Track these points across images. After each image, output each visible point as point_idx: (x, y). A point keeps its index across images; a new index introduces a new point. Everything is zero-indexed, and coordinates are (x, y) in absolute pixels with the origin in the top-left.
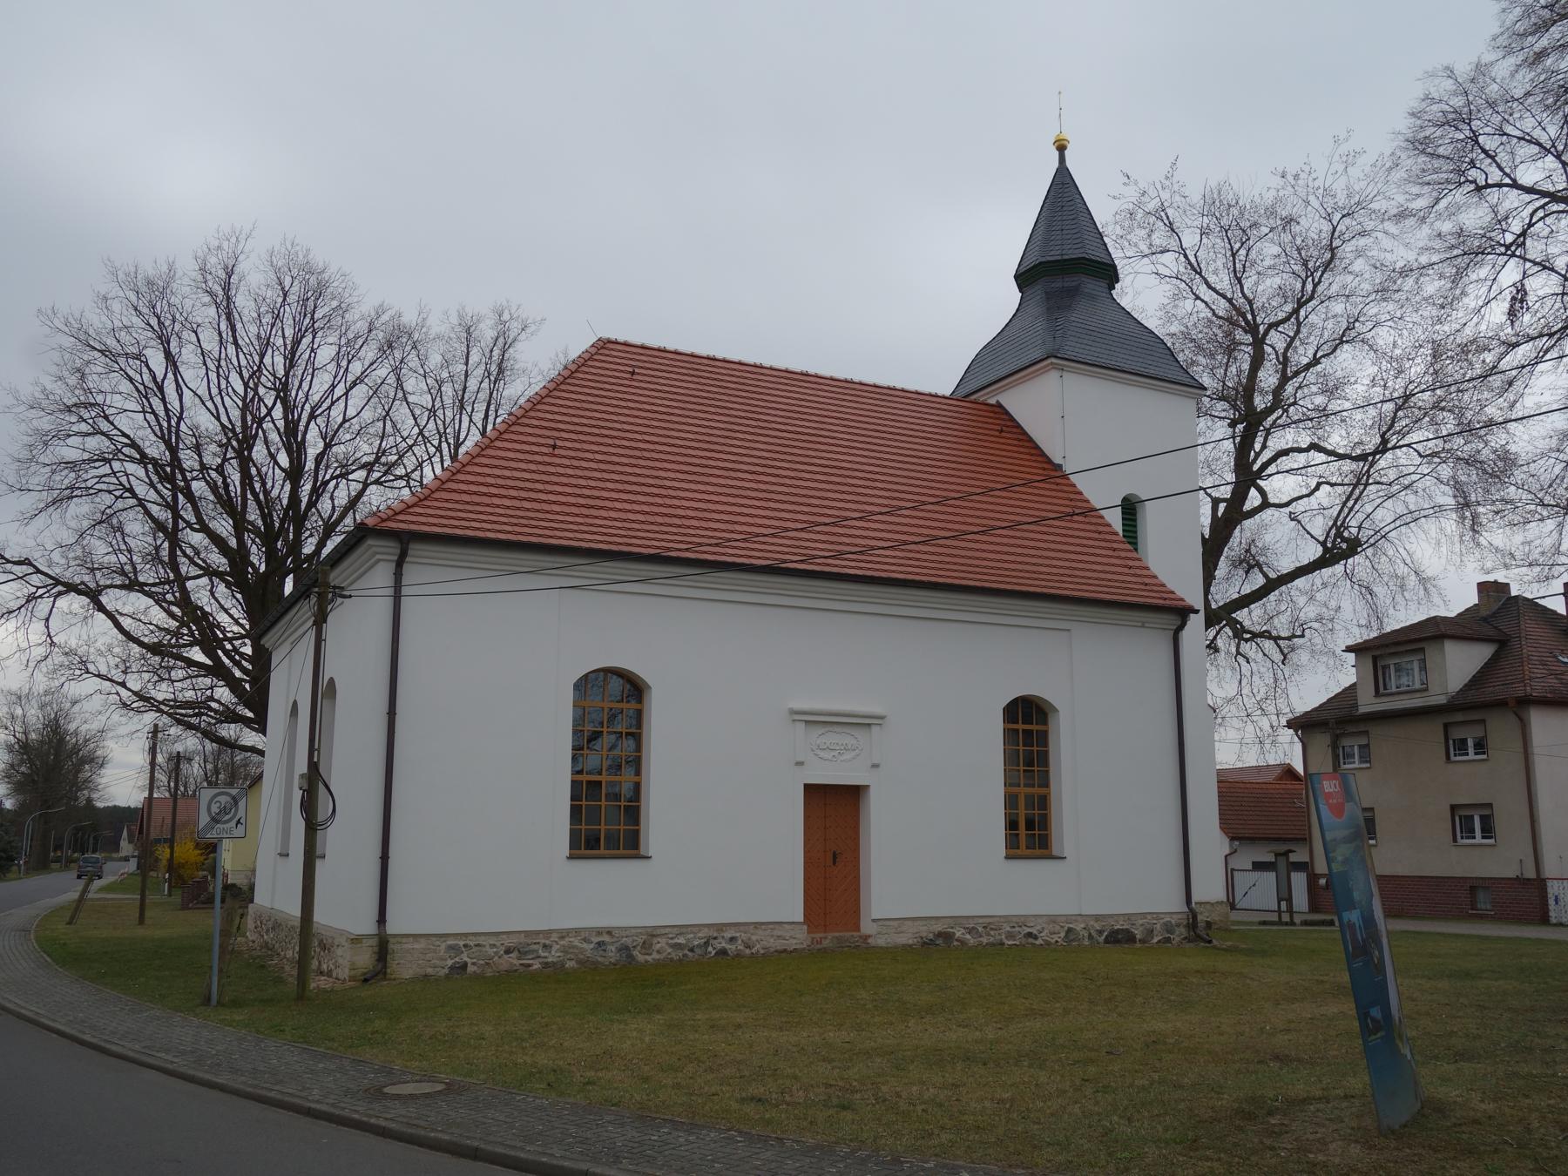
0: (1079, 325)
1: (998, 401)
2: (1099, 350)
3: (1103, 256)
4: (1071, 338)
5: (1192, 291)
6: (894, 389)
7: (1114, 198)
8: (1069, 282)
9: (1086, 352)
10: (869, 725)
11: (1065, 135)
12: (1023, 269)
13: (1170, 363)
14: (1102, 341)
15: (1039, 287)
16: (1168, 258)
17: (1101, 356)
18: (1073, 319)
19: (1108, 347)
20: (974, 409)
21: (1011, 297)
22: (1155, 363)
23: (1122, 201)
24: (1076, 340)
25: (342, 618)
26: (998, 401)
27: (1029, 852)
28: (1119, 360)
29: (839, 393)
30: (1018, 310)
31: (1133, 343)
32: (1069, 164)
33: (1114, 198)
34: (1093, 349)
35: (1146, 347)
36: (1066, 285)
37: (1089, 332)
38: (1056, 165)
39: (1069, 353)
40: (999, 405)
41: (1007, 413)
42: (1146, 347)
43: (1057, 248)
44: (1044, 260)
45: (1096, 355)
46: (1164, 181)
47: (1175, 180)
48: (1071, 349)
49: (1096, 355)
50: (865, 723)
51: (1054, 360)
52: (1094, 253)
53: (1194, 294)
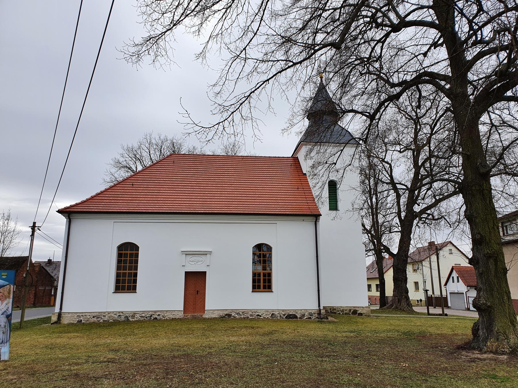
10: (207, 254)
27: (264, 290)
50: (205, 254)
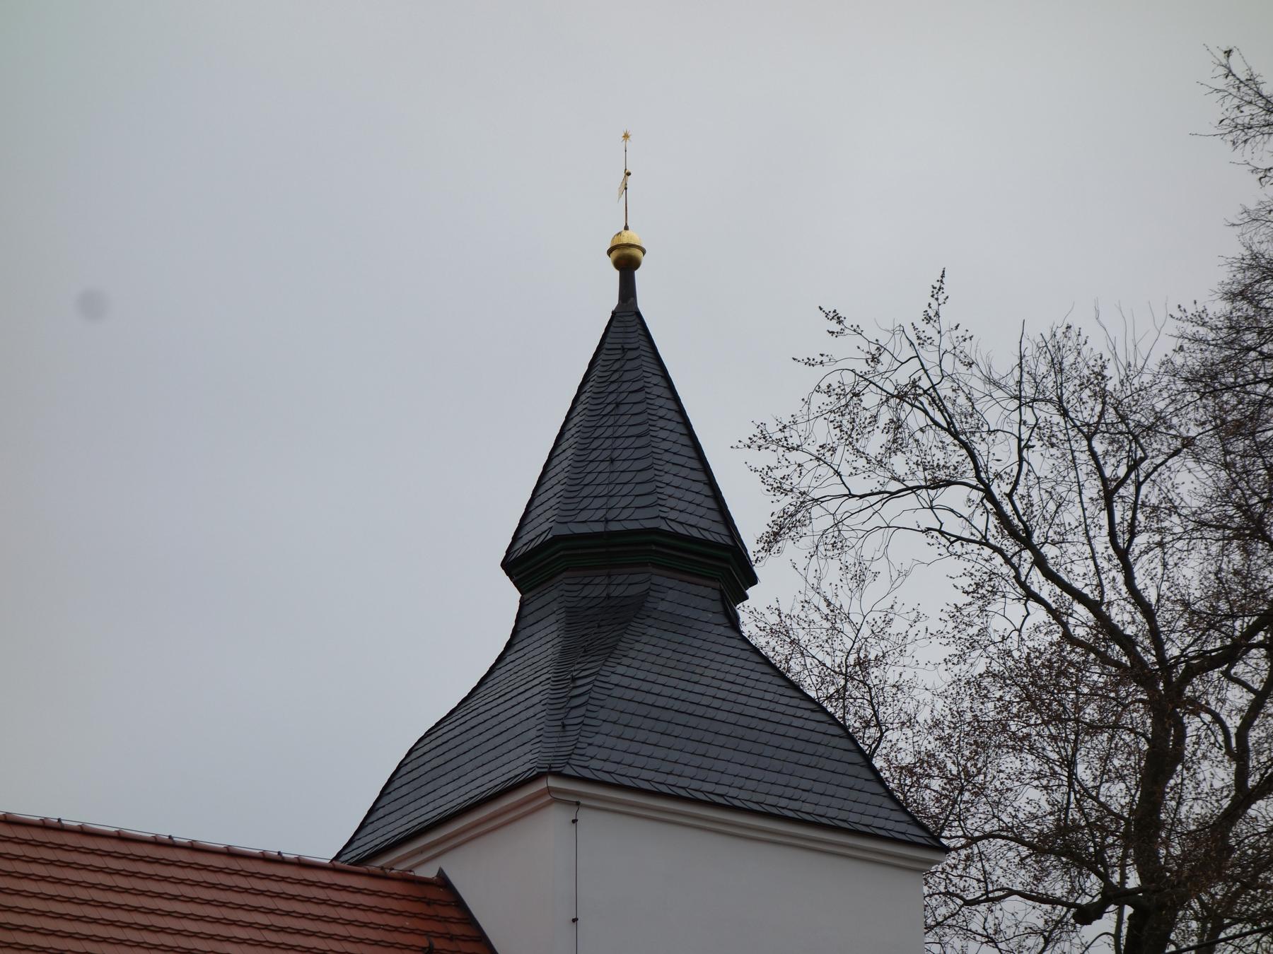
0: (629, 694)
1: (441, 874)
2: (674, 755)
3: (703, 523)
4: (606, 728)
5: (1017, 577)
6: (171, 844)
7: (810, 363)
8: (626, 585)
9: (640, 761)
11: (631, 237)
12: (521, 549)
13: (859, 784)
14: (687, 733)
15: (555, 594)
16: (954, 496)
17: (678, 769)
18: (615, 679)
19: (702, 749)
20: (374, 893)
21: (509, 597)
22: (819, 787)
23: (826, 369)
24: (618, 730)
25: (1193, 463)
26: (441, 874)
28: (726, 779)
29: (17, 858)
30: (509, 645)
31: (764, 737)
32: (645, 303)
33: (810, 363)
34: (660, 753)
35: (799, 746)
36: (617, 592)
37: (655, 713)
38: (613, 301)
39: (595, 764)
40: (443, 882)
41: (459, 903)
42: (799, 746)
43: (599, 502)
44: (563, 530)
45: (667, 767)
46: (922, 326)
47: (946, 322)
48: (603, 753)
49: (667, 767)
51: (552, 782)
52: (683, 517)
53: (1023, 585)
